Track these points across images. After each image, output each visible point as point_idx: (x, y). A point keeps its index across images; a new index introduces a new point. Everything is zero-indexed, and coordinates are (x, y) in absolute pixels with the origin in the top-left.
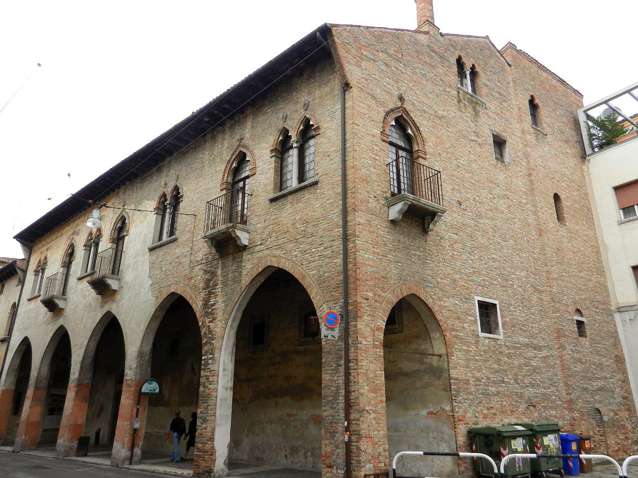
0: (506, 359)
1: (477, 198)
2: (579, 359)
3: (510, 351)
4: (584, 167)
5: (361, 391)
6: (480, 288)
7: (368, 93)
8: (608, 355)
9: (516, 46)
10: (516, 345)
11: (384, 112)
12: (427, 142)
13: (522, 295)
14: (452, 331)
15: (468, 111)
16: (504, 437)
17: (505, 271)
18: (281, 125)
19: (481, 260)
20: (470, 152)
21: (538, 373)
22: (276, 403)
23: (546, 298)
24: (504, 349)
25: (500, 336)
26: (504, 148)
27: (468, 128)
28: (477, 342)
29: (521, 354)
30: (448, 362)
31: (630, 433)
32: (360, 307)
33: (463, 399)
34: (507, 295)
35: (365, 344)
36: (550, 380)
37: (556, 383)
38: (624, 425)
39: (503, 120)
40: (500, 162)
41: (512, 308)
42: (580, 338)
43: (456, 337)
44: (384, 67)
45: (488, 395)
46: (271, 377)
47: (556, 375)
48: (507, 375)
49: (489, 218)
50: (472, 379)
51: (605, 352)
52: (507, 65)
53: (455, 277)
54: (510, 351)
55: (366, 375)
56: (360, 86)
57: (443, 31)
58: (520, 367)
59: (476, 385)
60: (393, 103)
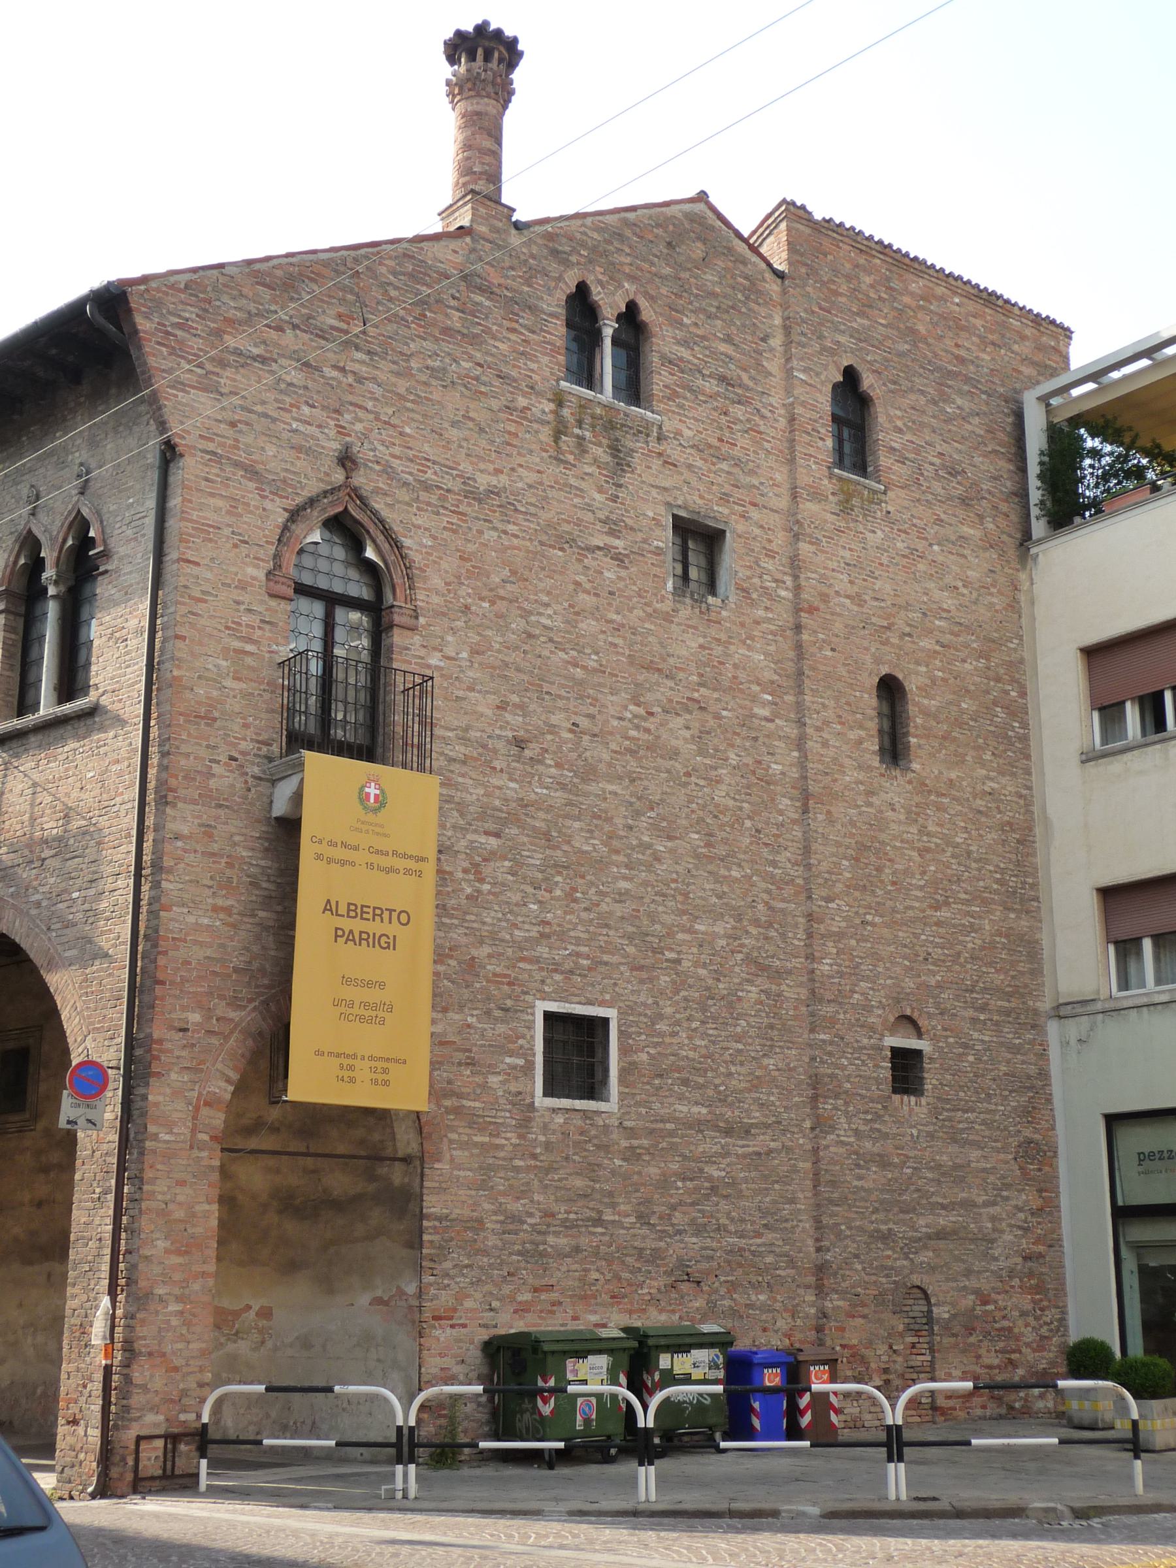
0: (618, 1162)
1: (584, 723)
2: (878, 1155)
3: (635, 1143)
4: (1023, 576)
5: (146, 1252)
6: (558, 977)
7: (237, 464)
8: (996, 1141)
9: (809, 208)
10: (661, 1125)
11: (285, 510)
12: (425, 579)
13: (708, 989)
14: (445, 1096)
15: (588, 458)
16: (545, 1353)
17: (653, 922)
18: (23, 523)
19: (575, 900)
20: (578, 584)
21: (726, 1197)
22: (49, 1275)
23: (792, 990)
24: (614, 1136)
25: (611, 1105)
26: (721, 551)
27: (580, 514)
28: (525, 1123)
29: (673, 1147)
30: (422, 1175)
31: (1024, 1350)
32: (161, 1051)
33: (455, 1266)
34: (650, 990)
35: (168, 1142)
36: (765, 1213)
37: (787, 1221)
38: (1010, 1329)
39: (724, 466)
40: (688, 601)
41: (661, 1026)
42: (896, 1098)
43: (457, 1111)
44: (295, 376)
45: (543, 1254)
46: (39, 1205)
47: (792, 1201)
48: (613, 1205)
49: (620, 778)
50: (494, 1218)
51: (987, 1133)
52: (768, 275)
53: (474, 952)
54: (635, 1143)
55: (163, 1213)
56: (211, 446)
57: (520, 216)
58: (664, 1184)
59: (504, 1233)
60: (315, 476)
